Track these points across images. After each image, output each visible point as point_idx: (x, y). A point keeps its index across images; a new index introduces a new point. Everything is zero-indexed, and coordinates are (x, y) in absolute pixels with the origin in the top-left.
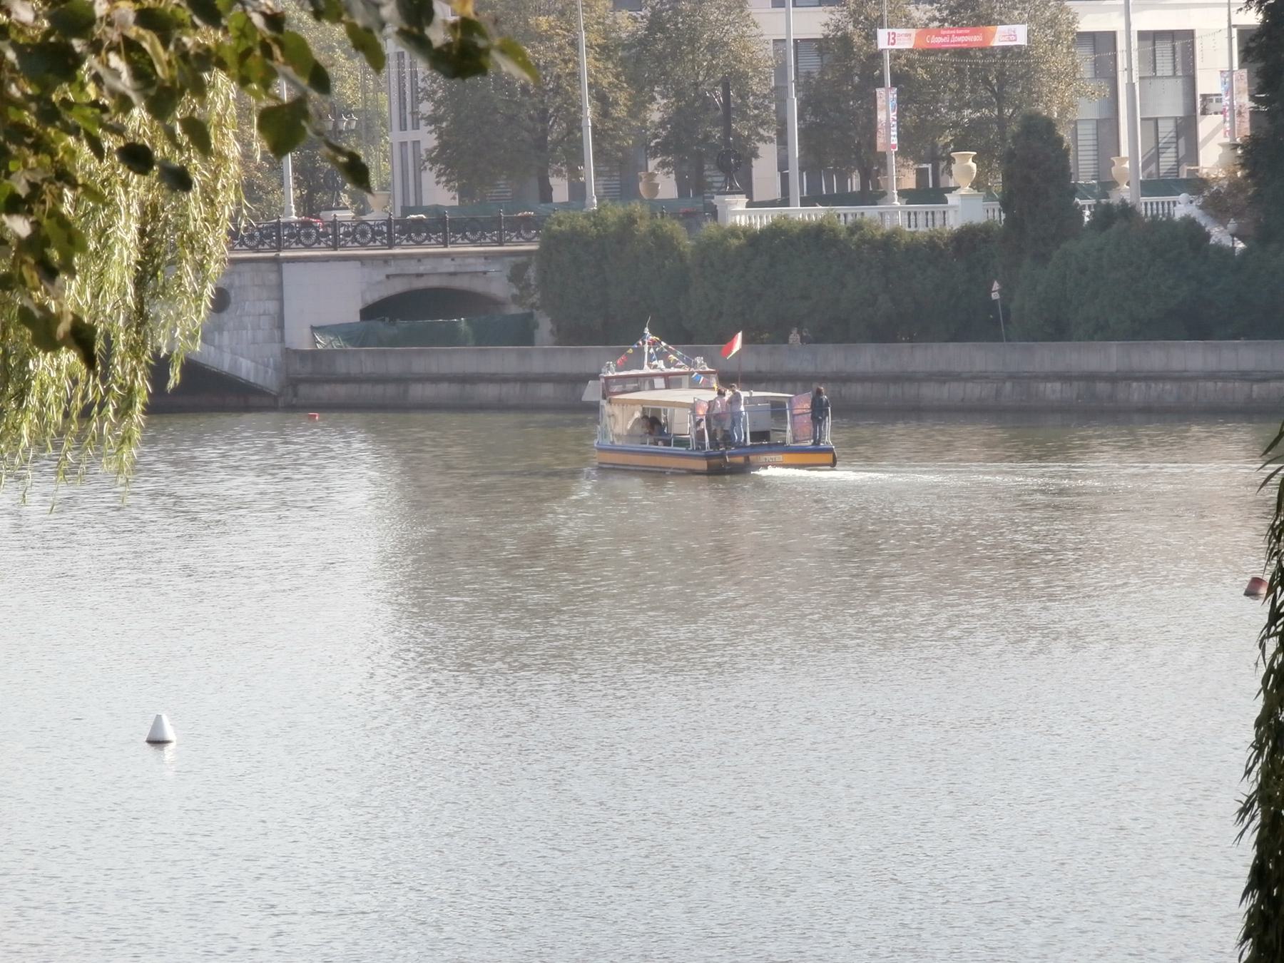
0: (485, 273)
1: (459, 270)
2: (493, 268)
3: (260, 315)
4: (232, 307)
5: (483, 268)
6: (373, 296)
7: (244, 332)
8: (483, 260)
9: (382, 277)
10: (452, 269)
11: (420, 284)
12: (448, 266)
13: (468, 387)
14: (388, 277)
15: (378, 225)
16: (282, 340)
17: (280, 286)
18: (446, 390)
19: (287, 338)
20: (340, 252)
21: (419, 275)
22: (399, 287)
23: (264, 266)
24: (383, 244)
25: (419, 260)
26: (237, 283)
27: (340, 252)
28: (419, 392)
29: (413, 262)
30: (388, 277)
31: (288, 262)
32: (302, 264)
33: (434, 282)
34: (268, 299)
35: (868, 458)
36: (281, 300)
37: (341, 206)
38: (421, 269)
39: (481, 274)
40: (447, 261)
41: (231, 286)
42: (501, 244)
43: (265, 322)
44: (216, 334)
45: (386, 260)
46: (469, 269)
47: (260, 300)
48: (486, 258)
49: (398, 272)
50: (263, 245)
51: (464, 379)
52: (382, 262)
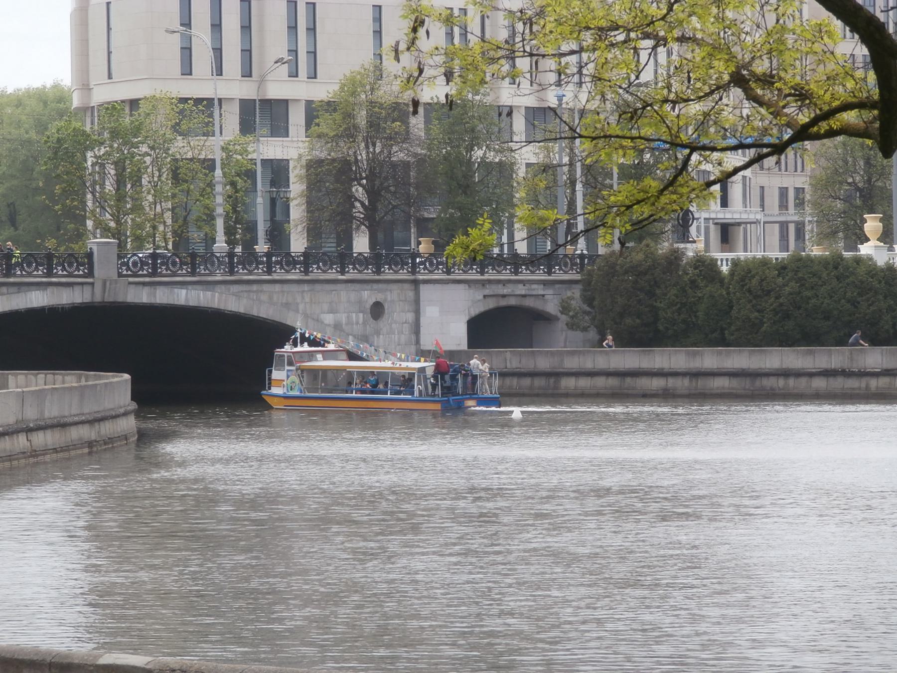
0: (543, 296)
1: (528, 293)
2: (549, 292)
3: (403, 323)
4: (386, 316)
5: (541, 292)
6: (476, 311)
7: (393, 336)
8: (542, 286)
9: (481, 297)
10: (523, 292)
11: (503, 303)
12: (521, 290)
13: (628, 380)
14: (485, 296)
15: (297, 257)
16: (418, 342)
17: (417, 301)
18: (657, 383)
19: (422, 342)
20: (12, 280)
21: (504, 296)
22: (491, 304)
23: (406, 286)
24: (264, 272)
25: (483, 285)
26: (389, 299)
27: (12, 280)
28: (569, 383)
29: (500, 286)
30: (485, 296)
31: (424, 283)
32: (440, 285)
33: (512, 302)
34: (409, 311)
35: (496, 435)
36: (417, 312)
37: (691, 239)
38: (505, 291)
39: (541, 297)
40: (521, 286)
41: (386, 300)
42: (516, 275)
43: (406, 329)
44: (376, 336)
45: (484, 283)
46: (534, 293)
47: (403, 312)
48: (544, 285)
49: (492, 293)
50: (38, 271)
51: (622, 374)
52: (481, 285)
